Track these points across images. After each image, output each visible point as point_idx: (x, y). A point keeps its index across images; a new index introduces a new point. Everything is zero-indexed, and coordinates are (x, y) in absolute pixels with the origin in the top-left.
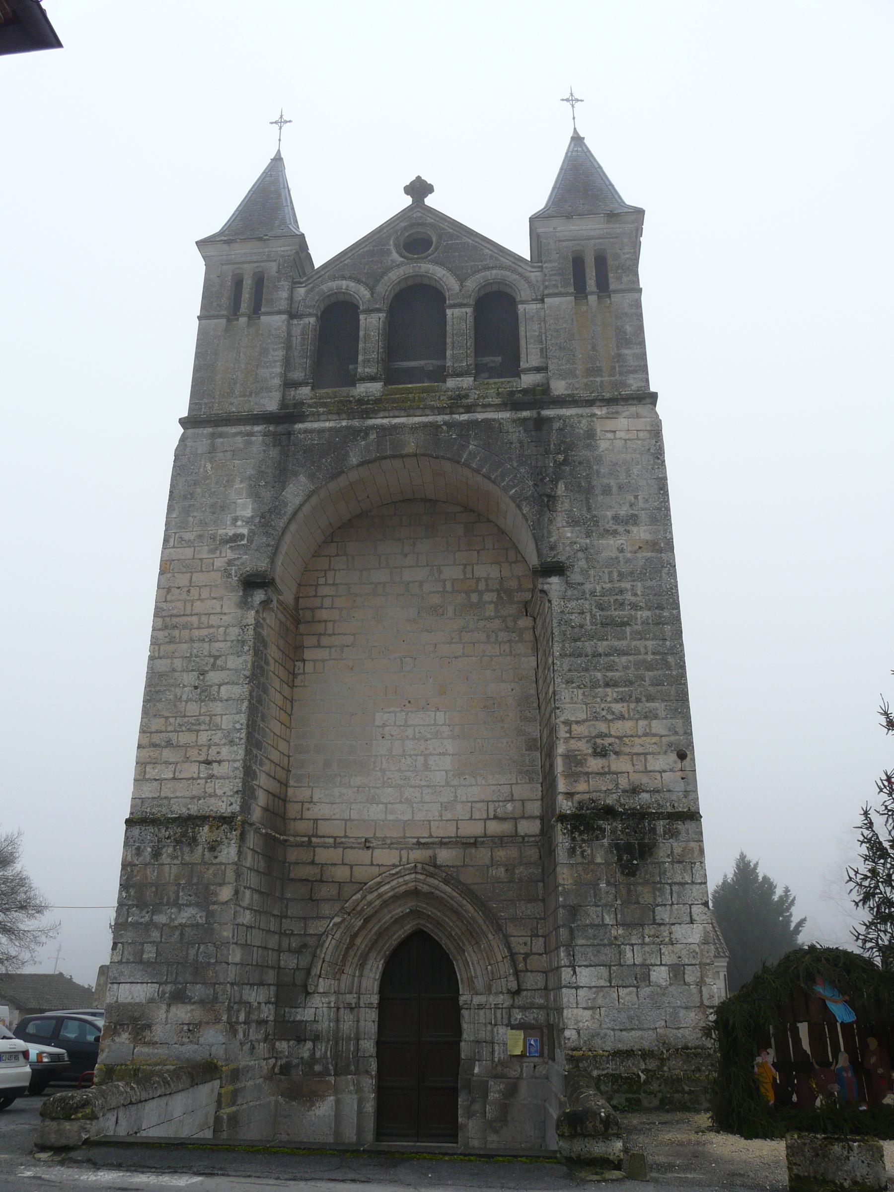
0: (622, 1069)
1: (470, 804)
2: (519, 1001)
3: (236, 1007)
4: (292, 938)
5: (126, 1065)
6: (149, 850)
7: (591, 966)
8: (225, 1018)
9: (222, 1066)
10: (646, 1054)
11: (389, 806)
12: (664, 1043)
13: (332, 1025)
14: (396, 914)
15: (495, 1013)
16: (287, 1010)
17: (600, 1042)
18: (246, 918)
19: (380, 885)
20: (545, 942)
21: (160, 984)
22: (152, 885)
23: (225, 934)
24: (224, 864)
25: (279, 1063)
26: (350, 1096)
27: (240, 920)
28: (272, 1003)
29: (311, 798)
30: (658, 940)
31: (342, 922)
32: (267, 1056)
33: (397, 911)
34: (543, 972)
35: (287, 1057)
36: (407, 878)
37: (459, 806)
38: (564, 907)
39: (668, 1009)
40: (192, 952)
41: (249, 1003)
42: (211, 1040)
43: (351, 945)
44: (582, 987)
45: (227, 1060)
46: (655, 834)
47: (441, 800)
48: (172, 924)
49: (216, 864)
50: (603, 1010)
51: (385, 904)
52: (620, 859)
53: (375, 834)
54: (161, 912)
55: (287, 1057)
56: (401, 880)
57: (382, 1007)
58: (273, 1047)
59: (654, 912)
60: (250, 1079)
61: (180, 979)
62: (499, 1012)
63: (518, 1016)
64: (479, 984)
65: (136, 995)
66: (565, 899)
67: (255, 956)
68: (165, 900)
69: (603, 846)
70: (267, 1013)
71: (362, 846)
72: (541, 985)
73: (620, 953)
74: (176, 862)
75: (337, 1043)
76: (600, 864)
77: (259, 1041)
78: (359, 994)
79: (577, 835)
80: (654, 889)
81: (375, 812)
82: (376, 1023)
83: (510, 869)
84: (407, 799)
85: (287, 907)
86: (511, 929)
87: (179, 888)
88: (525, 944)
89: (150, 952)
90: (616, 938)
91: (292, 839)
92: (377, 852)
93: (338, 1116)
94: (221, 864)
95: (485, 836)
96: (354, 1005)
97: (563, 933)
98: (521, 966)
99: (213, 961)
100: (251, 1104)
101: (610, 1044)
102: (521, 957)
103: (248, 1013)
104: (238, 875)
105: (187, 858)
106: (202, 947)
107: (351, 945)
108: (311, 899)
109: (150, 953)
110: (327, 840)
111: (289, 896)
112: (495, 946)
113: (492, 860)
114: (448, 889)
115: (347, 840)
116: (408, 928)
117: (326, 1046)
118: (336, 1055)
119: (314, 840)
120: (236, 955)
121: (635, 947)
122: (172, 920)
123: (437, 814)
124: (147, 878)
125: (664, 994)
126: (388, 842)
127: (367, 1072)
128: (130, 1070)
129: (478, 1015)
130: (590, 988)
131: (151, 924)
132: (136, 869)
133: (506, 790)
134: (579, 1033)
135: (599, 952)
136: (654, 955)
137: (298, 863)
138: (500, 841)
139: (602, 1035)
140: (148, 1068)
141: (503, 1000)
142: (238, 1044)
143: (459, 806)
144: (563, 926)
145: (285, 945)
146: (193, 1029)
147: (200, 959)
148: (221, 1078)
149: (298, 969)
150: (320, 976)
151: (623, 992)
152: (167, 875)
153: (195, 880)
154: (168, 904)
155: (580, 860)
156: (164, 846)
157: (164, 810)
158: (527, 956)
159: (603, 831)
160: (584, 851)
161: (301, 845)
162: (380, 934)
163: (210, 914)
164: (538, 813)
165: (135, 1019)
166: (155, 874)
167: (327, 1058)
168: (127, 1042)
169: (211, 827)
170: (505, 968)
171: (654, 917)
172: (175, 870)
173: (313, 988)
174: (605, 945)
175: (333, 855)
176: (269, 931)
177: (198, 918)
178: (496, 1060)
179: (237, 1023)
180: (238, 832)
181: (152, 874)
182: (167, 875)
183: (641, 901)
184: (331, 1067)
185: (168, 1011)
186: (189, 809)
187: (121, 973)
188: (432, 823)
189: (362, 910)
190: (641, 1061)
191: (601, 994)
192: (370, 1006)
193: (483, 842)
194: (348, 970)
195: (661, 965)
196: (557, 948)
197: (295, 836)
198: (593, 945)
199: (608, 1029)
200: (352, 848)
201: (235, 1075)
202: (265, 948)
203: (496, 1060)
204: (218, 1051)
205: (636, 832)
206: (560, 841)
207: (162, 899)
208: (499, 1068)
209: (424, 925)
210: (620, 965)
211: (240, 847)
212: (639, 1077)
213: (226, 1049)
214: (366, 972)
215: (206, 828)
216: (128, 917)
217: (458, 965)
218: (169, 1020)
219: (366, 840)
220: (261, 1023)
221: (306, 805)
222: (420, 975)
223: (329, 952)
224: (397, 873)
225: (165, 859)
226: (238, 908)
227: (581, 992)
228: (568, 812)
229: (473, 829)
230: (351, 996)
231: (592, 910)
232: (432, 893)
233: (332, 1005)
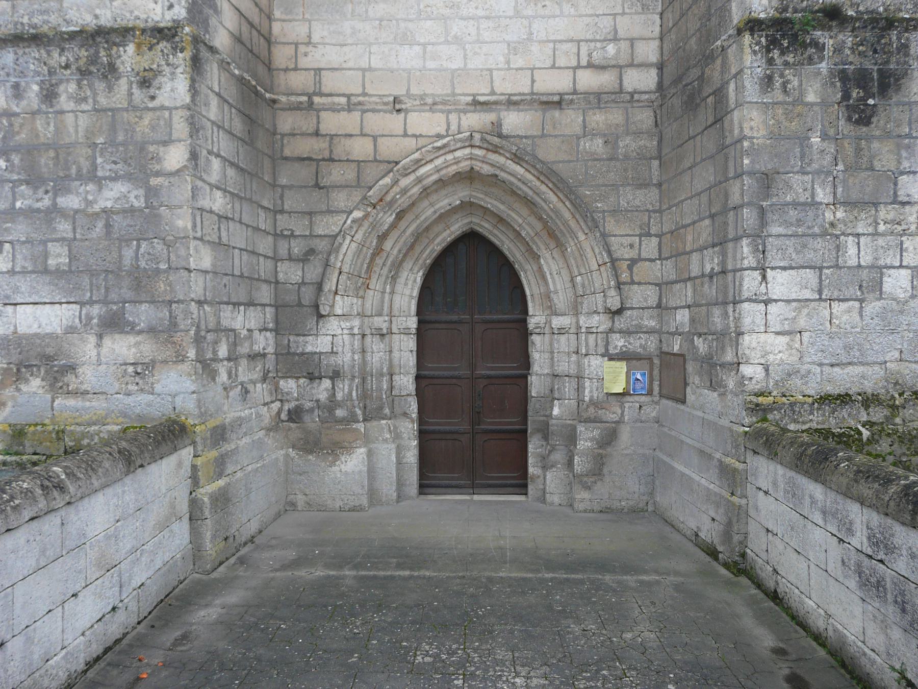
0: (833, 421)
1: (551, 45)
2: (621, 323)
3: (210, 337)
4: (292, 241)
5: (44, 425)
6: (36, 88)
7: (791, 268)
8: (192, 354)
9: (195, 425)
10: (869, 401)
11: (429, 48)
12: (896, 383)
13: (356, 357)
14: (441, 208)
15: (586, 339)
16: (292, 338)
17: (799, 382)
18: (218, 202)
19: (418, 163)
20: (660, 244)
21: (82, 304)
22: (48, 146)
23: (180, 223)
24: (167, 108)
25: (286, 408)
26: (386, 446)
27: (205, 203)
28: (271, 330)
29: (309, 37)
30: (899, 228)
31: (366, 216)
32: (268, 399)
33: (441, 204)
34: (656, 285)
35: (297, 400)
36: (458, 154)
37: (535, 48)
38: (751, 174)
39: (906, 334)
40: (128, 254)
41: (234, 330)
42: (173, 388)
43: (378, 251)
44: (776, 301)
45: (201, 415)
46: (907, 55)
47: (508, 38)
48: (90, 210)
49: (154, 109)
50: (806, 335)
51: (426, 192)
52: (846, 96)
53: (408, 90)
54: (68, 191)
55: (297, 400)
56: (450, 157)
57: (420, 334)
58: (277, 389)
59: (896, 184)
60: (245, 434)
61: (113, 296)
62: (592, 338)
63: (619, 343)
64: (561, 300)
65: (44, 322)
66: (752, 162)
67: (237, 261)
68: (74, 171)
69: (819, 73)
70: (264, 342)
71: (390, 107)
72: (653, 301)
73: (838, 248)
74: (84, 107)
75: (364, 380)
76: (812, 104)
77: (254, 383)
78: (391, 315)
79: (776, 53)
80: (899, 147)
81: (408, 57)
82: (415, 353)
83: (611, 140)
84: (456, 37)
85: (282, 197)
86: (610, 225)
87: (94, 152)
88: (631, 246)
89: (59, 255)
90: (832, 225)
91: (283, 99)
92: (413, 117)
93: (372, 472)
94: (162, 108)
95: (575, 92)
96: (385, 331)
97: (749, 216)
98: (625, 276)
99: (163, 266)
100: (250, 468)
101: (815, 385)
102: (624, 265)
103: (233, 346)
104: (195, 129)
105: (103, 101)
106: (144, 245)
107: (378, 251)
108: (317, 186)
109: (58, 256)
110: (336, 99)
111: (283, 181)
112: (589, 250)
113: (585, 127)
114: (519, 170)
115: (367, 98)
116: (456, 228)
117: (350, 386)
118: (364, 396)
119: (316, 99)
120: (204, 259)
121: (862, 239)
122: (89, 203)
123: (502, 59)
124: (37, 136)
125: (901, 312)
126: (429, 101)
127: (405, 414)
128: (50, 432)
129: (558, 341)
130: (788, 301)
131: (54, 211)
132: (17, 122)
133: (606, 23)
134: (767, 370)
135: (804, 246)
136: (891, 252)
137: (294, 135)
138: (597, 99)
139: (803, 372)
140: (78, 429)
141: (600, 322)
142: (220, 389)
143: (535, 48)
144: (749, 204)
145: (283, 252)
146: (142, 370)
147: (143, 264)
148: (194, 443)
149: (303, 283)
150: (336, 293)
151: (837, 307)
152: (71, 130)
153: (121, 138)
154: (79, 177)
155: (780, 97)
156: (61, 81)
157: (54, 19)
158: (633, 262)
159: (820, 48)
160: (788, 82)
161: (298, 107)
162: (417, 237)
163: (151, 193)
164: (654, 58)
165: (48, 359)
166: (52, 128)
167: (352, 400)
168: (41, 391)
169: (139, 46)
170: (603, 279)
171: (895, 193)
172: (84, 121)
173: (328, 308)
174: (814, 236)
175: (346, 122)
176: (257, 229)
177: (132, 199)
178: (587, 399)
179: (215, 359)
180: (188, 54)
181: (45, 129)
182: (71, 130)
183: (877, 165)
184: (359, 412)
185: (99, 345)
186: (96, 17)
187: (16, 290)
188: (495, 73)
189: (393, 201)
190: (862, 409)
191: (805, 311)
192: (406, 332)
193: (572, 100)
194: (376, 284)
195: (901, 266)
196: (737, 239)
197: (288, 95)
198: (794, 235)
199: (814, 363)
200: (374, 111)
201: (220, 434)
202: (253, 253)
203: (587, 399)
204: (187, 405)
205: (875, 51)
206: (748, 64)
207: (69, 169)
208: (592, 410)
209: (479, 225)
210: (837, 266)
211: (193, 81)
212: (860, 433)
213: (199, 401)
214: (399, 288)
215: (131, 48)
216: (14, 200)
217: (527, 277)
218: (102, 361)
219: (396, 100)
220: (253, 357)
221: (302, 49)
222: (473, 290)
223: (348, 259)
224: (444, 146)
225: (64, 102)
226: (199, 183)
227: (773, 308)
228: (762, 16)
229: (555, 83)
230: (381, 319)
231: (796, 180)
232: (496, 176)
233: (356, 331)
